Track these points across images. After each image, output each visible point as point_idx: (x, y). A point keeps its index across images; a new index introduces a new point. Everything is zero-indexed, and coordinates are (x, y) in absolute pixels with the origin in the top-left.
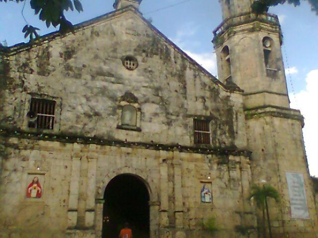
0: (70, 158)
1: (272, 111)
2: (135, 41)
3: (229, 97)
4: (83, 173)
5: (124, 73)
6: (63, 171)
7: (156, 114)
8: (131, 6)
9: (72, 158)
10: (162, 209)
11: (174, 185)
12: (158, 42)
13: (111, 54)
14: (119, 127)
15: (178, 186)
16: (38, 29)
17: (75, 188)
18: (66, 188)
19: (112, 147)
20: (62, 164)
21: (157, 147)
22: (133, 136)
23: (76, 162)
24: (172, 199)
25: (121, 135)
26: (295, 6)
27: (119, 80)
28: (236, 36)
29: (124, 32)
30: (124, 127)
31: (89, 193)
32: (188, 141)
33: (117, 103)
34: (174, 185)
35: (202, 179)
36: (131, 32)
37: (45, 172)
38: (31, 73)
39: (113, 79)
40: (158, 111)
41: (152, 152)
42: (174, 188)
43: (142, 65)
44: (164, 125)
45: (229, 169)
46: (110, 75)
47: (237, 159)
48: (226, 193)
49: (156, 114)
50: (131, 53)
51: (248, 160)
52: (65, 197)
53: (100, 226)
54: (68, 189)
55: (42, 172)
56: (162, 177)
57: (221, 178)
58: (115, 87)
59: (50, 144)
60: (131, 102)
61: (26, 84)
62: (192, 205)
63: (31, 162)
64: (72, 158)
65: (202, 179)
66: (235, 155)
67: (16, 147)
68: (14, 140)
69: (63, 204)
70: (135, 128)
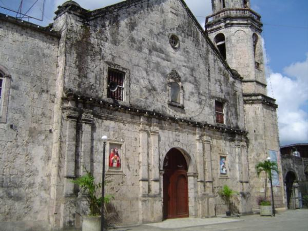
61: (103, 52)
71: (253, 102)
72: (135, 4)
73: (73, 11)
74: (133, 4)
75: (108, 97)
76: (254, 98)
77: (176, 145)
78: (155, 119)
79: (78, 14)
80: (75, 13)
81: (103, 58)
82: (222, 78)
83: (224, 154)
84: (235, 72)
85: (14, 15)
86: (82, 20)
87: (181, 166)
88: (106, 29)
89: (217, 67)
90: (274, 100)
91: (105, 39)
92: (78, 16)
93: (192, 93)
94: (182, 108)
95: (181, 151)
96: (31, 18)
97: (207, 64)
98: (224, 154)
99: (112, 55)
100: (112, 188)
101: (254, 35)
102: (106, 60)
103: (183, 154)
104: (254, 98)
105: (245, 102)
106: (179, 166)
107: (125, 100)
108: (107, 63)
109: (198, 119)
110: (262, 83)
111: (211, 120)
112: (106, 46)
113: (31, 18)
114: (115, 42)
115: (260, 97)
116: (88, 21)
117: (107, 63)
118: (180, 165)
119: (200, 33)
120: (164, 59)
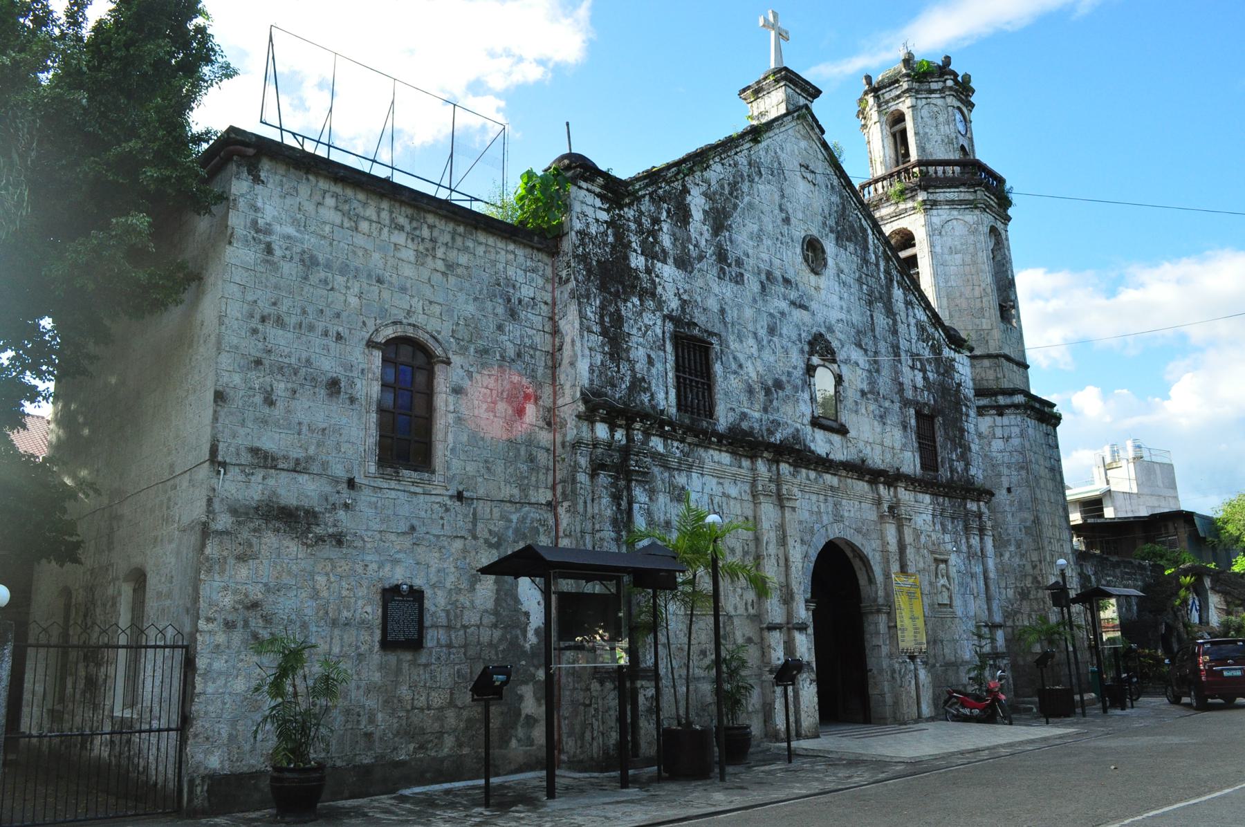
28: (934, 212)
41: (862, 487)
61: (659, 289)
70: (834, 425)
71: (1000, 410)
72: (722, 159)
73: (585, 181)
74: (717, 159)
75: (679, 409)
76: (1002, 400)
77: (835, 532)
78: (787, 466)
79: (598, 190)
80: (590, 187)
81: (660, 304)
82: (927, 354)
83: (941, 554)
84: (952, 332)
85: (443, 194)
86: (606, 206)
87: (42, 386)
88: (661, 229)
89: (912, 321)
90: (1053, 405)
91: (661, 256)
92: (599, 195)
93: (863, 393)
94: (842, 431)
95: (843, 546)
96: (476, 200)
97: (890, 312)
98: (941, 554)
99: (680, 299)
100: (701, 651)
101: (993, 230)
102: (666, 312)
103: (850, 554)
104: (1002, 400)
105: (981, 411)
106: (29, 378)
107: (723, 418)
108: (669, 317)
109: (877, 459)
110: (1017, 359)
111: (910, 462)
112: (666, 275)
113: (476, 200)
114: (683, 263)
115: (1019, 399)
116: (621, 208)
117: (669, 317)
118: (40, 375)
119: (869, 231)
120: (793, 303)
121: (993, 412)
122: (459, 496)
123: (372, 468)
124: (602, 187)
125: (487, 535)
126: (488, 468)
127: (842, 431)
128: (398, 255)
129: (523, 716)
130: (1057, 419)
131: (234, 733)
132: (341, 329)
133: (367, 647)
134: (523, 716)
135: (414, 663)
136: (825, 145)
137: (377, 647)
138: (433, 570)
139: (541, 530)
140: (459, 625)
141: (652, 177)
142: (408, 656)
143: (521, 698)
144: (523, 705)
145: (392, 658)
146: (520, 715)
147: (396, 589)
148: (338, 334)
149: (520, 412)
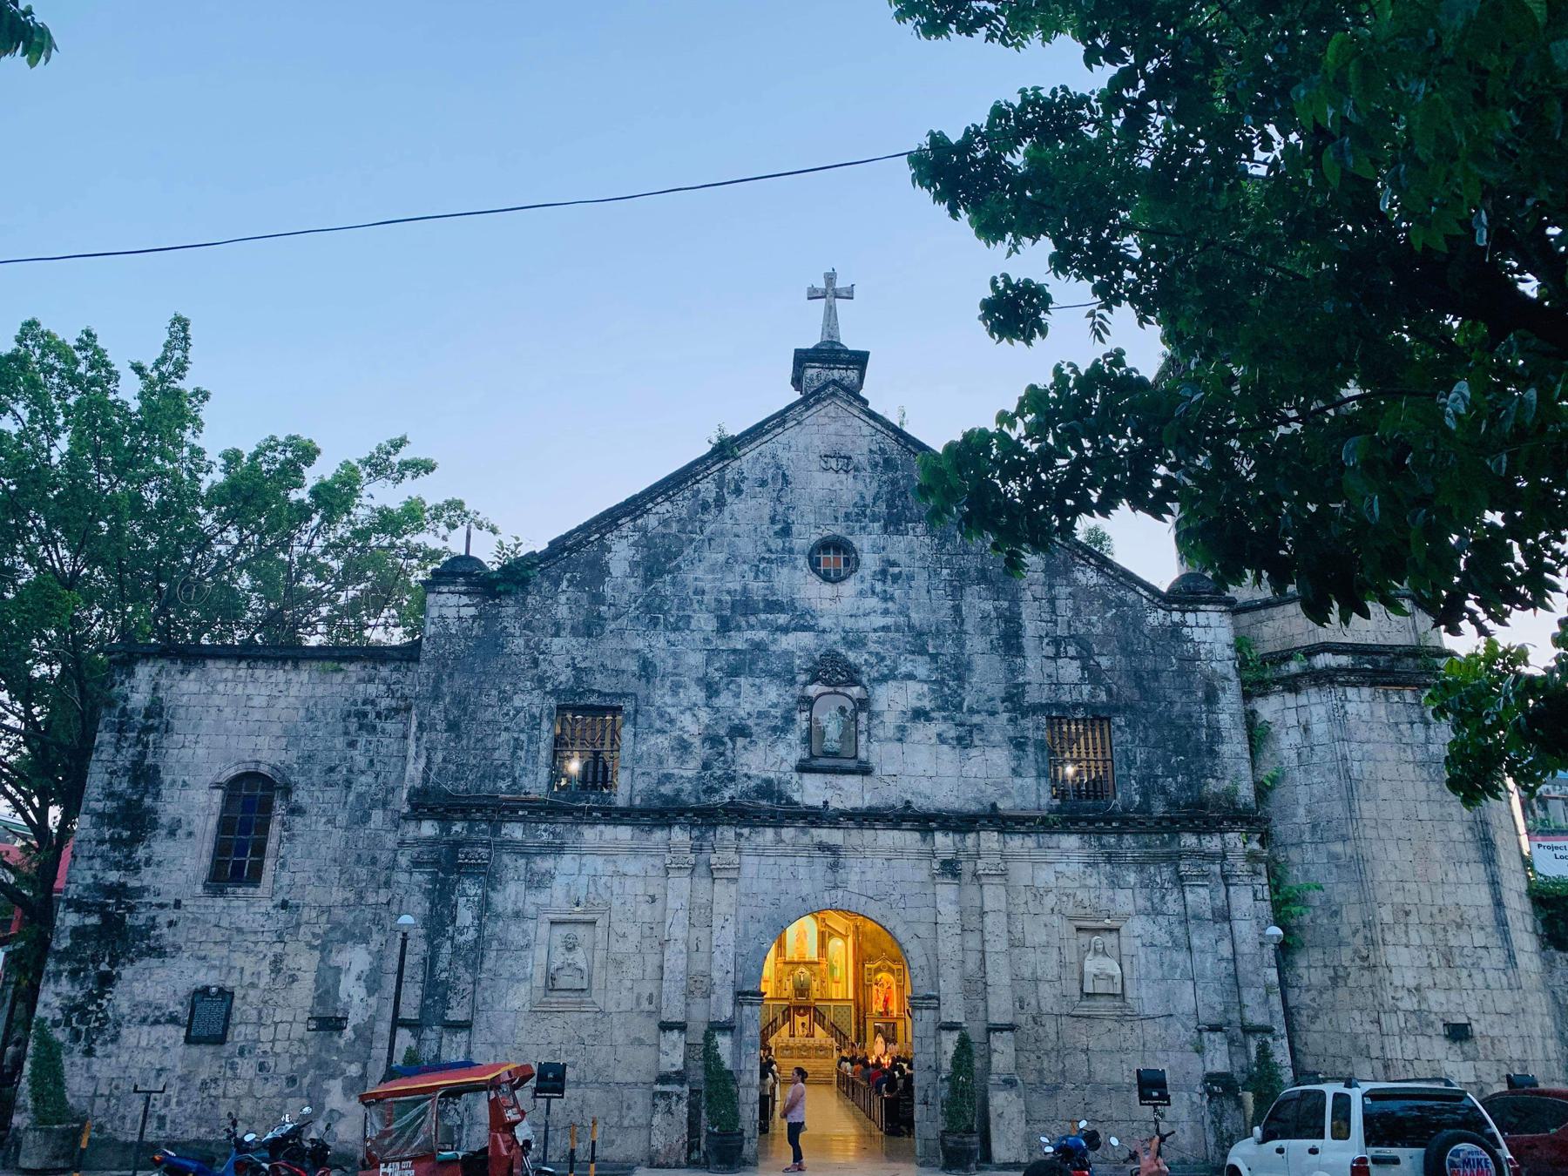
0: (662, 873)
1: (1333, 664)
2: (849, 489)
3: (1176, 629)
4: (701, 915)
5: (811, 591)
6: (645, 911)
7: (919, 714)
8: (834, 382)
9: (667, 870)
10: (945, 1019)
11: (983, 942)
12: (950, 495)
13: (777, 544)
14: (803, 768)
15: (997, 944)
16: (398, 444)
17: (675, 961)
18: (652, 960)
19: (784, 831)
20: (640, 891)
21: (925, 821)
22: (851, 793)
23: (681, 884)
24: (977, 987)
25: (812, 791)
26: (931, 134)
27: (803, 621)
29: (815, 467)
30: (815, 763)
31: (717, 975)
32: (1030, 794)
33: (797, 690)
34: (983, 942)
35: (1084, 918)
36: (833, 463)
37: (596, 916)
38: (557, 635)
39: (782, 619)
40: (927, 704)
41: (908, 839)
42: (983, 952)
43: (870, 562)
44: (945, 748)
45: (1180, 881)
46: (773, 606)
47: (1213, 843)
48: (383, 731)
49: (919, 714)
50: (838, 530)
51: (1255, 846)
52: (649, 988)
53: (751, 1072)
54: (657, 963)
55: (588, 917)
56: (940, 919)
57: (1154, 912)
58: (788, 642)
59: (609, 832)
60: (839, 684)
61: (543, 666)
62: (1048, 1004)
63: (558, 889)
64: (667, 870)
65: (1084, 918)
66: (1198, 832)
67: (519, 850)
68: (515, 831)
69: (645, 1006)
70: (852, 764)
80: (452, 588)
92: (464, 594)
99: (575, 668)
121: (1279, 688)
122: (284, 905)
123: (199, 889)
124: (466, 584)
125: (309, 938)
126: (320, 878)
127: (865, 770)
128: (250, 703)
129: (327, 1110)
130: (250, 778)
131: (165, 1166)
132: (187, 778)
133: (172, 1041)
134: (327, 1110)
135: (216, 1056)
136: (873, 415)
137: (182, 1039)
138: (247, 973)
139: (374, 929)
140: (269, 1022)
141: (559, 547)
142: (210, 1049)
143: (328, 1091)
144: (328, 1099)
145: (195, 1051)
146: (323, 1108)
147: (205, 990)
148: (184, 782)
149: (366, 818)
